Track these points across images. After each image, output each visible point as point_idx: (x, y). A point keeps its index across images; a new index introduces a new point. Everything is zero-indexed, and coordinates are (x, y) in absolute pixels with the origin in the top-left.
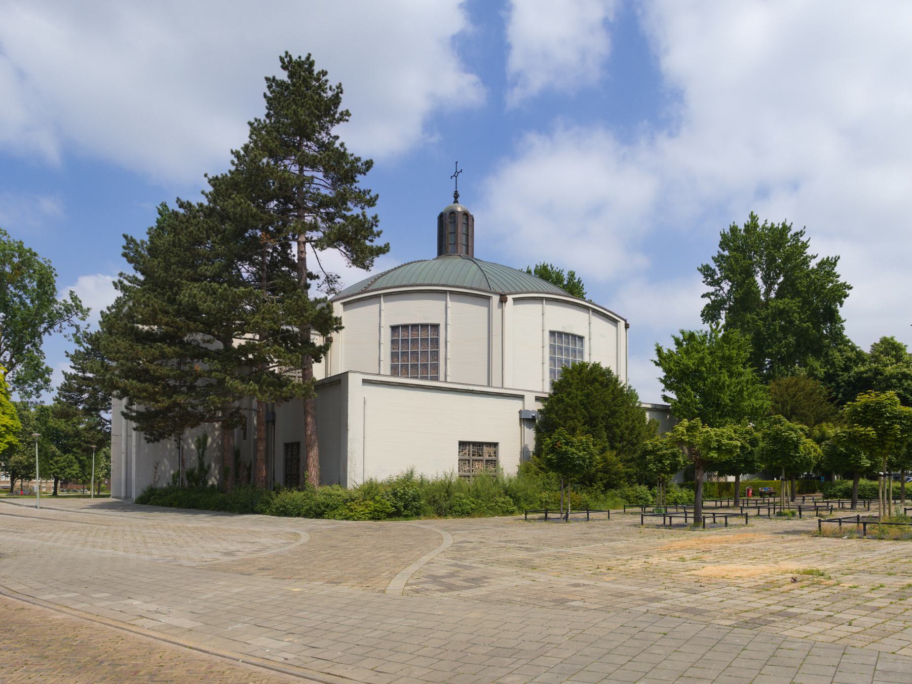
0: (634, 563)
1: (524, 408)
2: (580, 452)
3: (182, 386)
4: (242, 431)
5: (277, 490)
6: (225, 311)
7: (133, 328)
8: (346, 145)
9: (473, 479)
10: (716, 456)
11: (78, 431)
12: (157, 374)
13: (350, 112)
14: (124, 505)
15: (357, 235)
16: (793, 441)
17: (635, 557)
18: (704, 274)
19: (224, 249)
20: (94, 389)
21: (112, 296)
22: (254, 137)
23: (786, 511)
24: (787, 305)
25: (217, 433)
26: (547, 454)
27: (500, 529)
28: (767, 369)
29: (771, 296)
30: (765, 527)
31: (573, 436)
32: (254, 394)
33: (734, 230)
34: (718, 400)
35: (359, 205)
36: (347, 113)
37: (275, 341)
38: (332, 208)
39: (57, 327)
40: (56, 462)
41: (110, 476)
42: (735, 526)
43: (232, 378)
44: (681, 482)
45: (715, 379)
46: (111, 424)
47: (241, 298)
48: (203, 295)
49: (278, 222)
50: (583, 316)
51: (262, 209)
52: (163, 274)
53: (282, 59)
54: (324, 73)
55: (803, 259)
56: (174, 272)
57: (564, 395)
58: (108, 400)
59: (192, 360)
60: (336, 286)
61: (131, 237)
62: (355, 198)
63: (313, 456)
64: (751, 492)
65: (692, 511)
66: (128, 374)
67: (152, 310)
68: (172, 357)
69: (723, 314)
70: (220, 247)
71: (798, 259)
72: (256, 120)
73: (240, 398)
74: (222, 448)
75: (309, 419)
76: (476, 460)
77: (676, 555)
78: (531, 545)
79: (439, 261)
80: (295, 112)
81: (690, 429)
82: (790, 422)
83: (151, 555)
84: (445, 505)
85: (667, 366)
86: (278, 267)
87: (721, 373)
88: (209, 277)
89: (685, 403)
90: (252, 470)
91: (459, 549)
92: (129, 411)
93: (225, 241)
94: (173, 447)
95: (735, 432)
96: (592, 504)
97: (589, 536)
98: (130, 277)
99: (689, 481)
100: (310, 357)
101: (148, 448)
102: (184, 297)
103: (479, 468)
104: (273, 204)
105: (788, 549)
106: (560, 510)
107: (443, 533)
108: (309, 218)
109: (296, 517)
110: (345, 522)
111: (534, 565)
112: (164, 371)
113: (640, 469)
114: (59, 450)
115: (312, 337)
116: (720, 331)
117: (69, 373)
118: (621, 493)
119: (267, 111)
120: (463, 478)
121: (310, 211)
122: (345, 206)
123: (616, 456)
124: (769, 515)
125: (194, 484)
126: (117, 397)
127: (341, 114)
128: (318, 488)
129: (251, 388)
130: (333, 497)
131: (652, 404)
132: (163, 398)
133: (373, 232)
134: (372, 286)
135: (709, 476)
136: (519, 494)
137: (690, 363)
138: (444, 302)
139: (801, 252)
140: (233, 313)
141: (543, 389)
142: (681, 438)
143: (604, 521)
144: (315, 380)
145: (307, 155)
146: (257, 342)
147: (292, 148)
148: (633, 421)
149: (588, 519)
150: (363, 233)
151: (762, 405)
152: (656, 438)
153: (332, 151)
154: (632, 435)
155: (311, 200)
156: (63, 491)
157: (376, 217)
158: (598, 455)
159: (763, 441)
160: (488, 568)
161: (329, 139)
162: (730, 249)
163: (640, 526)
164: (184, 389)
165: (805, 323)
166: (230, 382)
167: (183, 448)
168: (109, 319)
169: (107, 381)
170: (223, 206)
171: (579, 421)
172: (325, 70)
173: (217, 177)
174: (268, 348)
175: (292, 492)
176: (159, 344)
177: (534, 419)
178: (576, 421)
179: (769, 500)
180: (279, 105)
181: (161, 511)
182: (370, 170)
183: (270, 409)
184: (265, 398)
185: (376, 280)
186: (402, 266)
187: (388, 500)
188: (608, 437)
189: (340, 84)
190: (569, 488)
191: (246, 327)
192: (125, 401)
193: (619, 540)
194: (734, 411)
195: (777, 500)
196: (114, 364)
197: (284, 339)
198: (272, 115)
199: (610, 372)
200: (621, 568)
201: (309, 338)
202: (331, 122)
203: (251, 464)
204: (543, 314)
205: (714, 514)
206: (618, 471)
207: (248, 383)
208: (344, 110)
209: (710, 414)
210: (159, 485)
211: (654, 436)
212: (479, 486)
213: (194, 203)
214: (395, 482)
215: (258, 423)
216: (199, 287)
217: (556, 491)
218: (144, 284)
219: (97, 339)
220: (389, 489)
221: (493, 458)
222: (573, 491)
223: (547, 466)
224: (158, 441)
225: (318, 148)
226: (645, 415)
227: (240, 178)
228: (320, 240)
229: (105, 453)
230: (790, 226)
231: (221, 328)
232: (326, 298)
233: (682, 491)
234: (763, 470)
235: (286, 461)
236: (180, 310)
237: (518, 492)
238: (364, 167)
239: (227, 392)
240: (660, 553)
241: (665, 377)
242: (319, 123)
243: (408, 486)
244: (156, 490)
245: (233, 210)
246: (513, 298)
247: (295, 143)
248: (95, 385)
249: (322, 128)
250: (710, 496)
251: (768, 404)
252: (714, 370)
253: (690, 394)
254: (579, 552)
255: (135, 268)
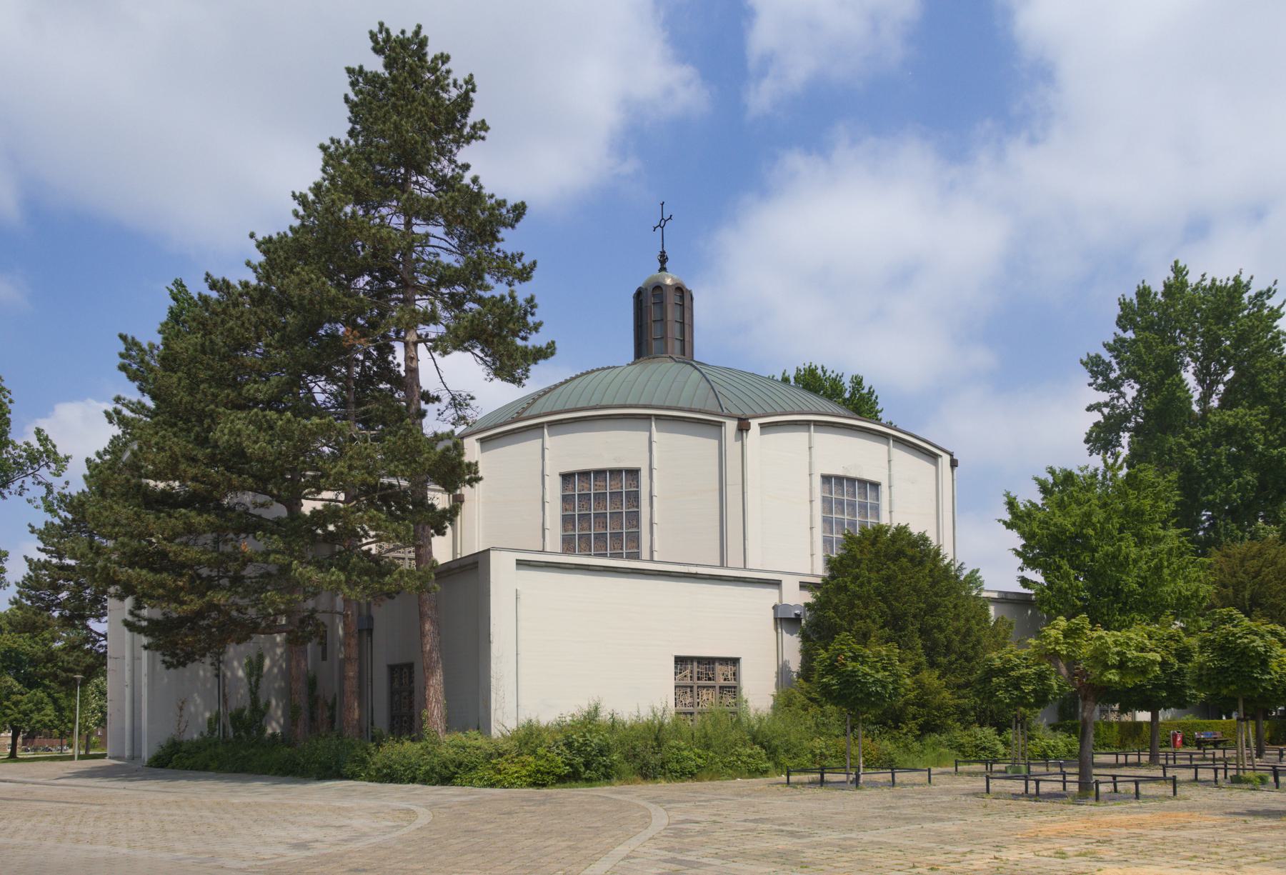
0: (976, 860)
1: (781, 601)
2: (878, 672)
3: (222, 577)
4: (320, 648)
5: (378, 740)
6: (288, 457)
7: (139, 486)
8: (481, 181)
9: (699, 717)
10: (1117, 679)
11: (52, 653)
12: (180, 558)
13: (488, 123)
14: (126, 771)
15: (501, 329)
16: (1258, 653)
17: (977, 848)
18: (1091, 371)
19: (285, 356)
20: (78, 584)
21: (102, 435)
22: (330, 170)
23: (1249, 774)
24: (1241, 419)
25: (279, 651)
26: (823, 676)
27: (745, 799)
28: (1204, 529)
29: (1211, 404)
30: (1211, 802)
31: (865, 647)
32: (338, 588)
33: (1143, 293)
34: (1117, 584)
35: (505, 280)
36: (483, 126)
37: (371, 503)
38: (459, 285)
39: (15, 486)
40: (16, 704)
41: (106, 724)
42: (1154, 797)
43: (302, 563)
44: (1054, 720)
45: (1111, 549)
46: (106, 639)
47: (314, 435)
48: (253, 431)
49: (372, 310)
50: (877, 449)
51: (344, 288)
52: (187, 399)
53: (373, 36)
54: (445, 58)
55: (1272, 338)
56: (205, 394)
57: (848, 579)
58: (101, 602)
59: (237, 534)
60: (468, 412)
61: (133, 338)
62: (498, 268)
63: (435, 688)
64: (1179, 739)
65: (1076, 770)
66: (133, 559)
67: (171, 457)
68: (205, 532)
69: (1125, 438)
70: (278, 353)
71: (1263, 337)
72: (332, 141)
73: (315, 595)
74: (287, 675)
75: (428, 626)
76: (704, 687)
77: (1050, 846)
78: (798, 826)
79: (638, 368)
80: (397, 127)
81: (1069, 633)
82: (1251, 620)
83: (174, 851)
84: (654, 760)
85: (1027, 529)
86: (373, 384)
87: (1121, 539)
88: (262, 402)
89: (1060, 590)
90: (337, 709)
91: (679, 834)
92: (136, 619)
93: (285, 342)
94: (209, 674)
95: (1150, 638)
96: (899, 758)
97: (897, 811)
98: (133, 404)
99: (1067, 719)
100: (427, 527)
101: (167, 676)
102: (221, 435)
103: (709, 699)
104: (362, 281)
105: (1258, 844)
106: (845, 768)
107: (652, 807)
108: (422, 304)
109: (408, 783)
110: (488, 790)
111: (805, 860)
112: (192, 553)
113: (982, 700)
114: (20, 682)
115: (430, 494)
116: (1120, 468)
117: (36, 560)
118: (949, 740)
119: (351, 125)
120: (682, 717)
121: (424, 291)
122: (480, 283)
123: (939, 678)
124: (1216, 781)
125: (243, 734)
126: (115, 596)
127: (474, 127)
128: (443, 736)
129: (333, 578)
130: (468, 750)
131: (1000, 592)
132: (192, 597)
133: (528, 324)
134: (530, 409)
135: (1103, 711)
136: (776, 742)
137: (1067, 523)
138: (648, 434)
139: (1267, 326)
140: (302, 458)
141: (812, 570)
142: (1054, 649)
143: (921, 788)
144: (437, 563)
145: (418, 199)
146: (341, 505)
147: (392, 187)
148: (967, 620)
149: (893, 783)
150: (511, 325)
151: (1197, 591)
152: (1008, 648)
153: (459, 190)
154: (965, 643)
155: (424, 273)
156: (26, 750)
157: (532, 299)
158: (908, 676)
159: (1201, 652)
160: (728, 865)
161: (453, 170)
162: (1135, 326)
163: (984, 796)
164: (225, 582)
165: (1275, 448)
166: (298, 569)
167: (224, 676)
168: (101, 472)
169: (99, 570)
170: (282, 285)
171: (874, 621)
172: (445, 53)
173: (270, 238)
174: (360, 513)
175: (403, 743)
176: (183, 511)
177: (797, 619)
178: (868, 621)
179: (1214, 754)
180: (370, 114)
181: (189, 779)
182: (522, 220)
183: (364, 612)
184: (356, 594)
185: (535, 400)
186: (577, 377)
187: (558, 754)
188: (924, 646)
189: (471, 75)
190: (861, 732)
191: (323, 480)
192: (129, 602)
193: (949, 819)
194: (1147, 602)
195: (1229, 754)
196: (110, 544)
197: (385, 500)
198: (359, 133)
199: (927, 539)
200: (954, 867)
201: (425, 497)
202: (457, 142)
203: (335, 699)
204: (810, 448)
205: (1114, 777)
206: (942, 704)
207: (328, 570)
208: (478, 119)
209: (1103, 607)
210: (186, 737)
211: (1004, 645)
212: (710, 729)
213: (234, 281)
214: (569, 725)
215: (346, 634)
216: (245, 418)
217: (837, 736)
218: (157, 415)
219: (82, 504)
220: (560, 737)
221: (732, 683)
222: (866, 737)
223: (823, 695)
224: (184, 665)
225: (435, 186)
226: (987, 610)
227: (308, 239)
228: (441, 338)
229: (97, 686)
230: (1249, 282)
231: (282, 484)
232: (452, 432)
233: (1056, 736)
234: (1202, 702)
235: (392, 693)
236: (215, 455)
237: (774, 738)
238: (512, 215)
239: (294, 586)
240: (1020, 842)
241: (1024, 546)
242: (437, 143)
243: (590, 731)
244: (180, 744)
245: (297, 292)
246: (760, 424)
247: (397, 178)
248: (79, 578)
249: (442, 152)
250: (1105, 746)
251: (1207, 590)
252: (1109, 533)
253: (1067, 575)
254: (880, 839)
255: (140, 389)
